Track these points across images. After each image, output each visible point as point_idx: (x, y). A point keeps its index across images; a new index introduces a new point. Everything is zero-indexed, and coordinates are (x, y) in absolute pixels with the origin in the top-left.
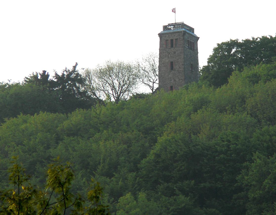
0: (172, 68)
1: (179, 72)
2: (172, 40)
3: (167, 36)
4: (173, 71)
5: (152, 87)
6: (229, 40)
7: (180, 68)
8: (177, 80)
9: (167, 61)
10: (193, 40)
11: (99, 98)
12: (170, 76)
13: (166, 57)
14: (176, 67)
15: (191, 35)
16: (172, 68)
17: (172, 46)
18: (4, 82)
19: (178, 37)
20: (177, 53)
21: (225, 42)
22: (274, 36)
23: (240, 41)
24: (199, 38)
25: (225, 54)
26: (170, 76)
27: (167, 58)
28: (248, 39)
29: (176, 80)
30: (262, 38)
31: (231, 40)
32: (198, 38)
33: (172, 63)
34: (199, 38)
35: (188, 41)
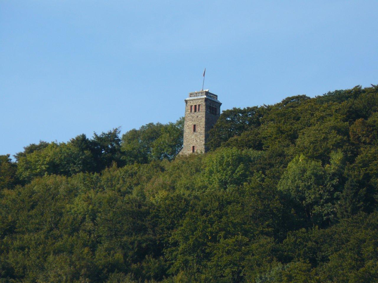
0: (194, 130)
1: (200, 134)
2: (195, 106)
3: (192, 102)
4: (195, 133)
5: (330, 102)
6: (327, 93)
7: (201, 130)
8: (199, 141)
9: (191, 124)
10: (215, 106)
11: (25, 184)
12: (193, 137)
13: (190, 120)
14: (198, 129)
15: (214, 101)
16: (194, 130)
17: (195, 111)
18: (120, 129)
19: (200, 104)
20: (199, 116)
21: (244, 109)
22: (376, 85)
23: (242, 109)
24: (222, 104)
25: (102, 151)
26: (193, 137)
27: (191, 121)
28: (169, 123)
29: (198, 141)
30: (87, 140)
31: (30, 145)
32: (220, 104)
33: (195, 126)
34: (222, 104)
35: (210, 106)
